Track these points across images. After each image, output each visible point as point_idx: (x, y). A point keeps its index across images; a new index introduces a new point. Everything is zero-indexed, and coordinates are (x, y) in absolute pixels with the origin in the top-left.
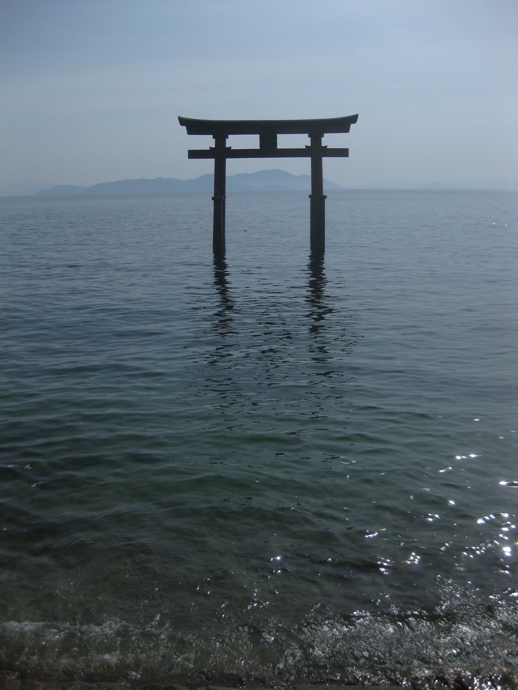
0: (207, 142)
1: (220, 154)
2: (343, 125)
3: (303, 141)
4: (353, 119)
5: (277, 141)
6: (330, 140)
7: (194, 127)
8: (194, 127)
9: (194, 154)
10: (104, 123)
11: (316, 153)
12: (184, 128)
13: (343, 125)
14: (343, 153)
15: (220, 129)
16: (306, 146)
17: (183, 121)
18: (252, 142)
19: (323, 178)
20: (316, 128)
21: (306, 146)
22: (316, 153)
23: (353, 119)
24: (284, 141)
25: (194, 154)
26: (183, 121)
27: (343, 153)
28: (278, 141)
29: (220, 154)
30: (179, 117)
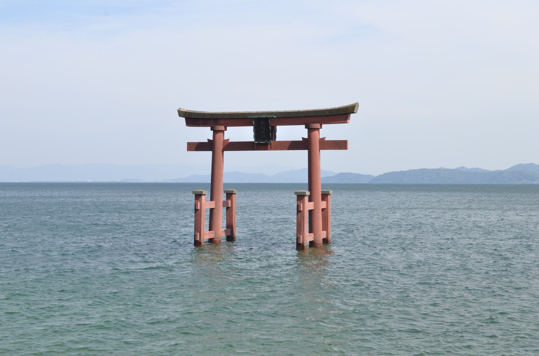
0: (204, 134)
2: (341, 115)
3: (299, 132)
5: (525, 163)
6: (329, 131)
7: (193, 119)
8: (193, 119)
10: (104, 106)
12: (183, 119)
13: (341, 115)
14: (341, 145)
15: (217, 121)
16: (303, 138)
17: (181, 114)
18: (246, 133)
19: (367, 183)
20: (312, 119)
21: (303, 138)
24: (285, 133)
26: (181, 114)
27: (341, 145)
28: (277, 134)
30: (357, 104)
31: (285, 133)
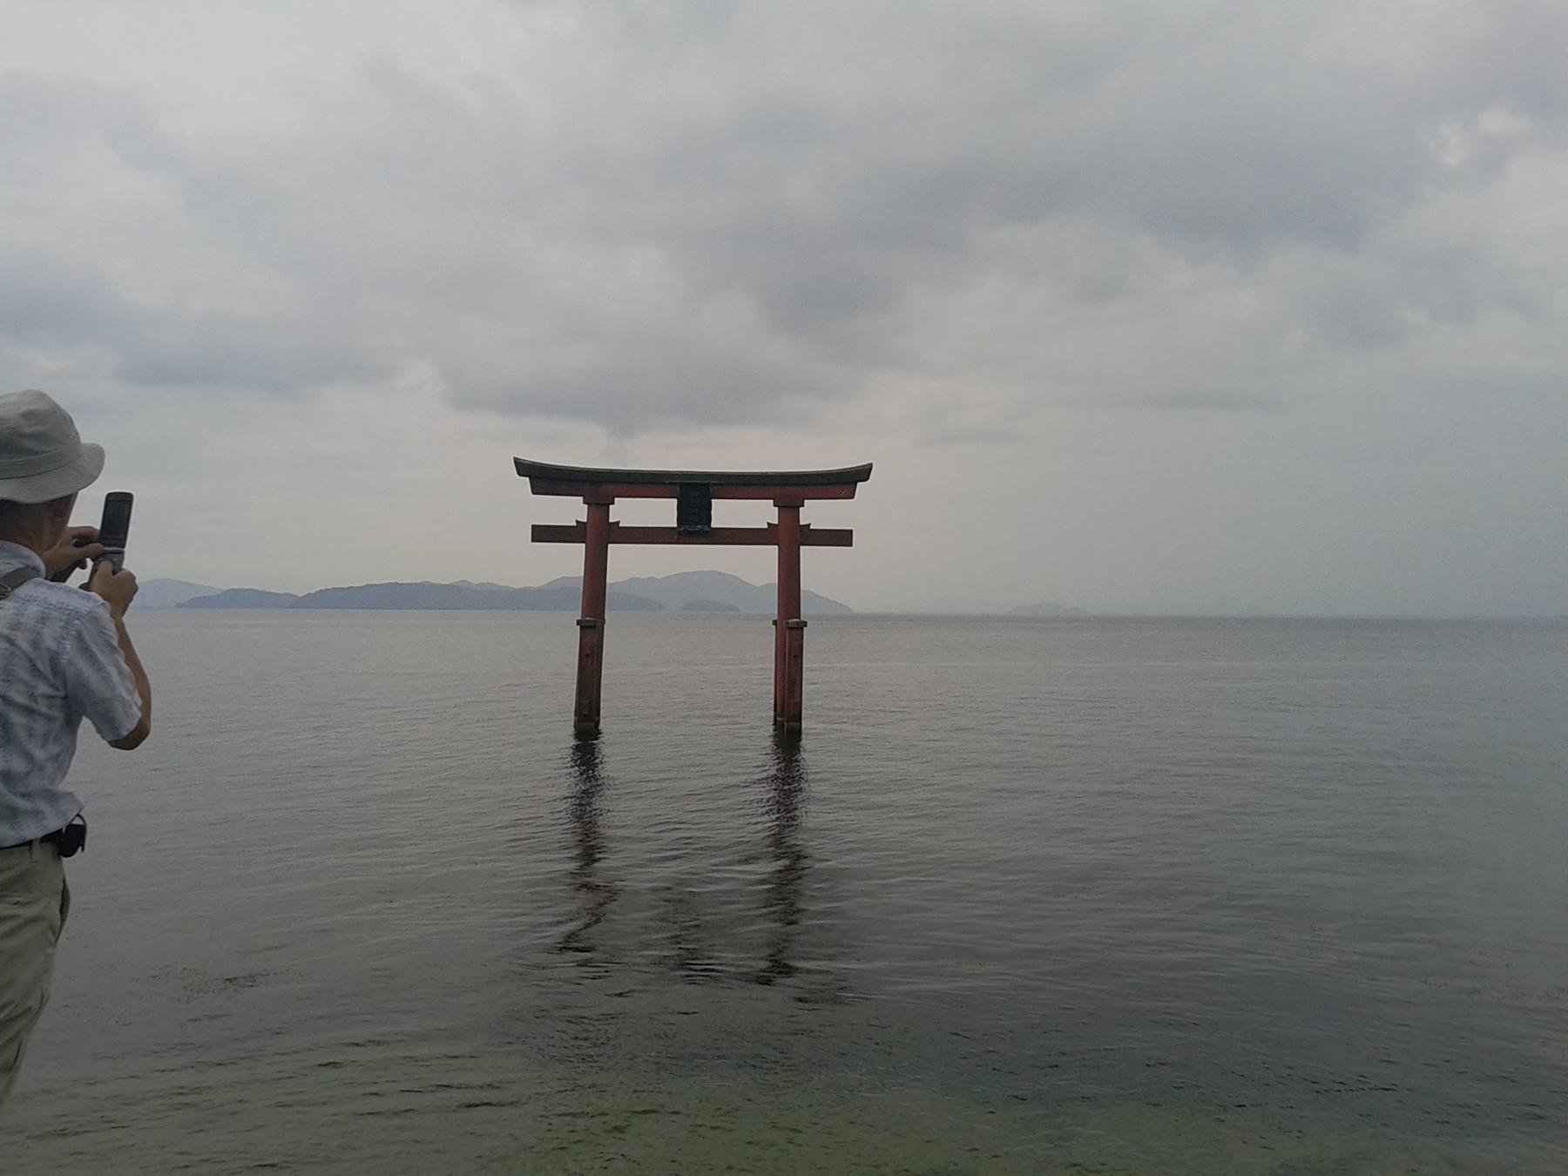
0: (570, 510)
1: (598, 536)
2: (842, 483)
3: (762, 513)
4: (864, 473)
6: (815, 513)
7: (546, 479)
8: (546, 479)
9: (542, 534)
11: (790, 538)
13: (842, 483)
14: (842, 538)
15: (599, 487)
17: (523, 468)
18: (664, 512)
20: (789, 489)
22: (790, 538)
23: (864, 473)
24: (724, 513)
25: (542, 534)
26: (523, 468)
27: (842, 538)
29: (598, 536)
31: (724, 513)
